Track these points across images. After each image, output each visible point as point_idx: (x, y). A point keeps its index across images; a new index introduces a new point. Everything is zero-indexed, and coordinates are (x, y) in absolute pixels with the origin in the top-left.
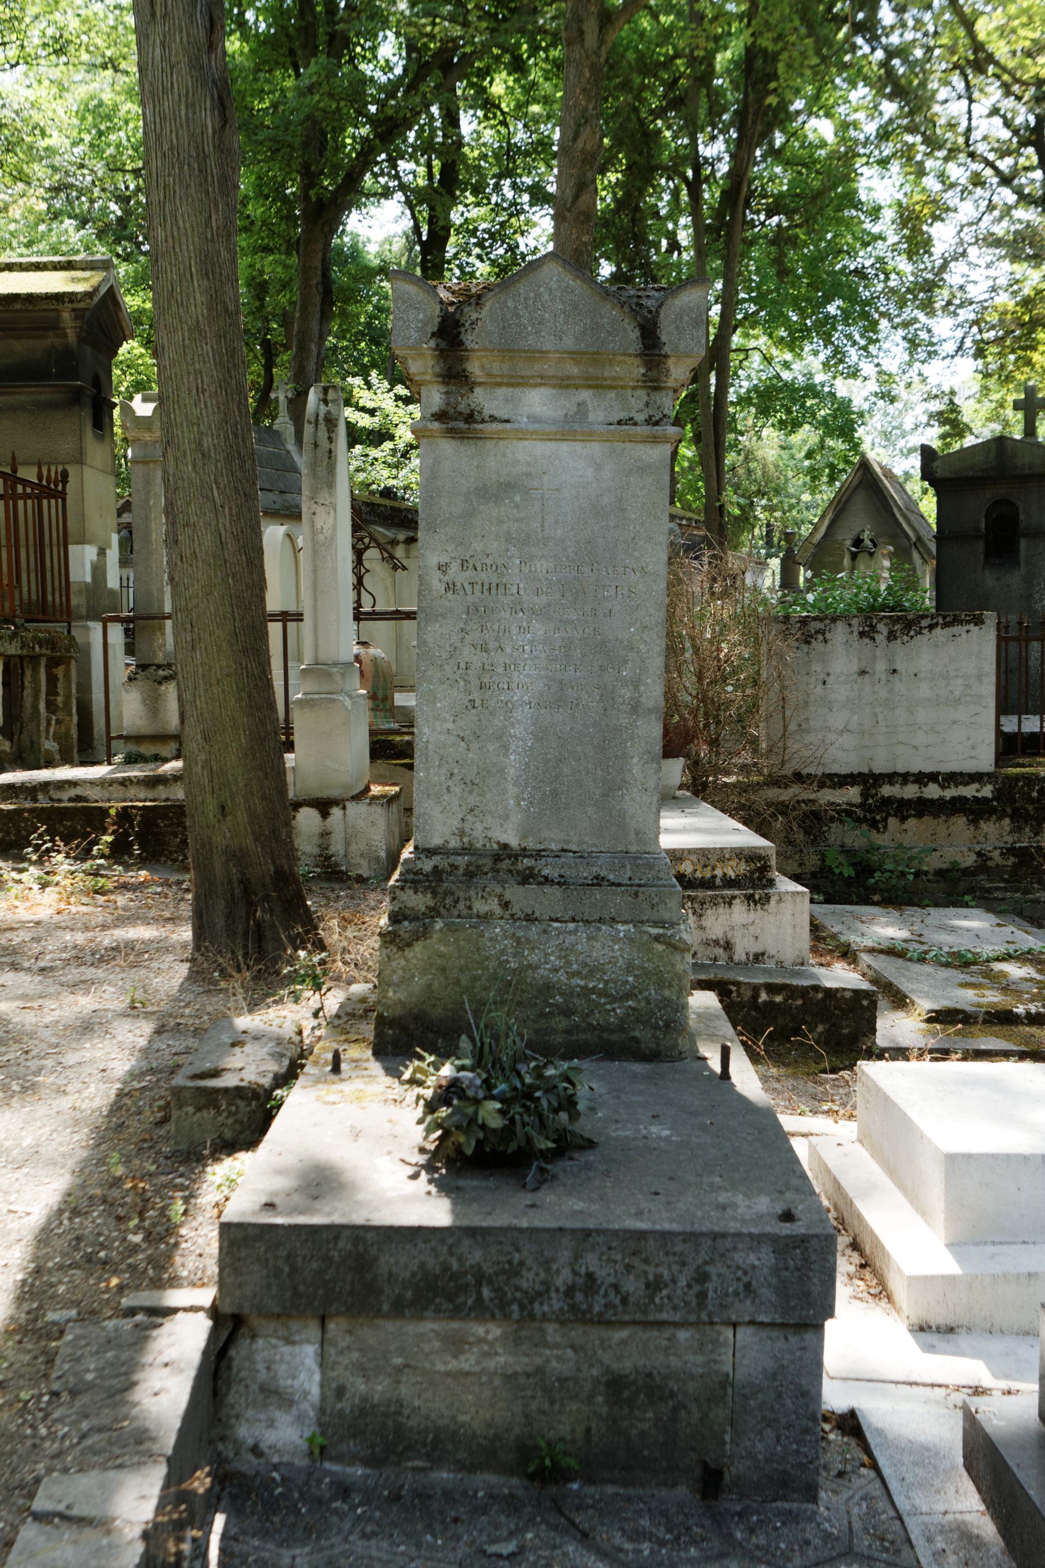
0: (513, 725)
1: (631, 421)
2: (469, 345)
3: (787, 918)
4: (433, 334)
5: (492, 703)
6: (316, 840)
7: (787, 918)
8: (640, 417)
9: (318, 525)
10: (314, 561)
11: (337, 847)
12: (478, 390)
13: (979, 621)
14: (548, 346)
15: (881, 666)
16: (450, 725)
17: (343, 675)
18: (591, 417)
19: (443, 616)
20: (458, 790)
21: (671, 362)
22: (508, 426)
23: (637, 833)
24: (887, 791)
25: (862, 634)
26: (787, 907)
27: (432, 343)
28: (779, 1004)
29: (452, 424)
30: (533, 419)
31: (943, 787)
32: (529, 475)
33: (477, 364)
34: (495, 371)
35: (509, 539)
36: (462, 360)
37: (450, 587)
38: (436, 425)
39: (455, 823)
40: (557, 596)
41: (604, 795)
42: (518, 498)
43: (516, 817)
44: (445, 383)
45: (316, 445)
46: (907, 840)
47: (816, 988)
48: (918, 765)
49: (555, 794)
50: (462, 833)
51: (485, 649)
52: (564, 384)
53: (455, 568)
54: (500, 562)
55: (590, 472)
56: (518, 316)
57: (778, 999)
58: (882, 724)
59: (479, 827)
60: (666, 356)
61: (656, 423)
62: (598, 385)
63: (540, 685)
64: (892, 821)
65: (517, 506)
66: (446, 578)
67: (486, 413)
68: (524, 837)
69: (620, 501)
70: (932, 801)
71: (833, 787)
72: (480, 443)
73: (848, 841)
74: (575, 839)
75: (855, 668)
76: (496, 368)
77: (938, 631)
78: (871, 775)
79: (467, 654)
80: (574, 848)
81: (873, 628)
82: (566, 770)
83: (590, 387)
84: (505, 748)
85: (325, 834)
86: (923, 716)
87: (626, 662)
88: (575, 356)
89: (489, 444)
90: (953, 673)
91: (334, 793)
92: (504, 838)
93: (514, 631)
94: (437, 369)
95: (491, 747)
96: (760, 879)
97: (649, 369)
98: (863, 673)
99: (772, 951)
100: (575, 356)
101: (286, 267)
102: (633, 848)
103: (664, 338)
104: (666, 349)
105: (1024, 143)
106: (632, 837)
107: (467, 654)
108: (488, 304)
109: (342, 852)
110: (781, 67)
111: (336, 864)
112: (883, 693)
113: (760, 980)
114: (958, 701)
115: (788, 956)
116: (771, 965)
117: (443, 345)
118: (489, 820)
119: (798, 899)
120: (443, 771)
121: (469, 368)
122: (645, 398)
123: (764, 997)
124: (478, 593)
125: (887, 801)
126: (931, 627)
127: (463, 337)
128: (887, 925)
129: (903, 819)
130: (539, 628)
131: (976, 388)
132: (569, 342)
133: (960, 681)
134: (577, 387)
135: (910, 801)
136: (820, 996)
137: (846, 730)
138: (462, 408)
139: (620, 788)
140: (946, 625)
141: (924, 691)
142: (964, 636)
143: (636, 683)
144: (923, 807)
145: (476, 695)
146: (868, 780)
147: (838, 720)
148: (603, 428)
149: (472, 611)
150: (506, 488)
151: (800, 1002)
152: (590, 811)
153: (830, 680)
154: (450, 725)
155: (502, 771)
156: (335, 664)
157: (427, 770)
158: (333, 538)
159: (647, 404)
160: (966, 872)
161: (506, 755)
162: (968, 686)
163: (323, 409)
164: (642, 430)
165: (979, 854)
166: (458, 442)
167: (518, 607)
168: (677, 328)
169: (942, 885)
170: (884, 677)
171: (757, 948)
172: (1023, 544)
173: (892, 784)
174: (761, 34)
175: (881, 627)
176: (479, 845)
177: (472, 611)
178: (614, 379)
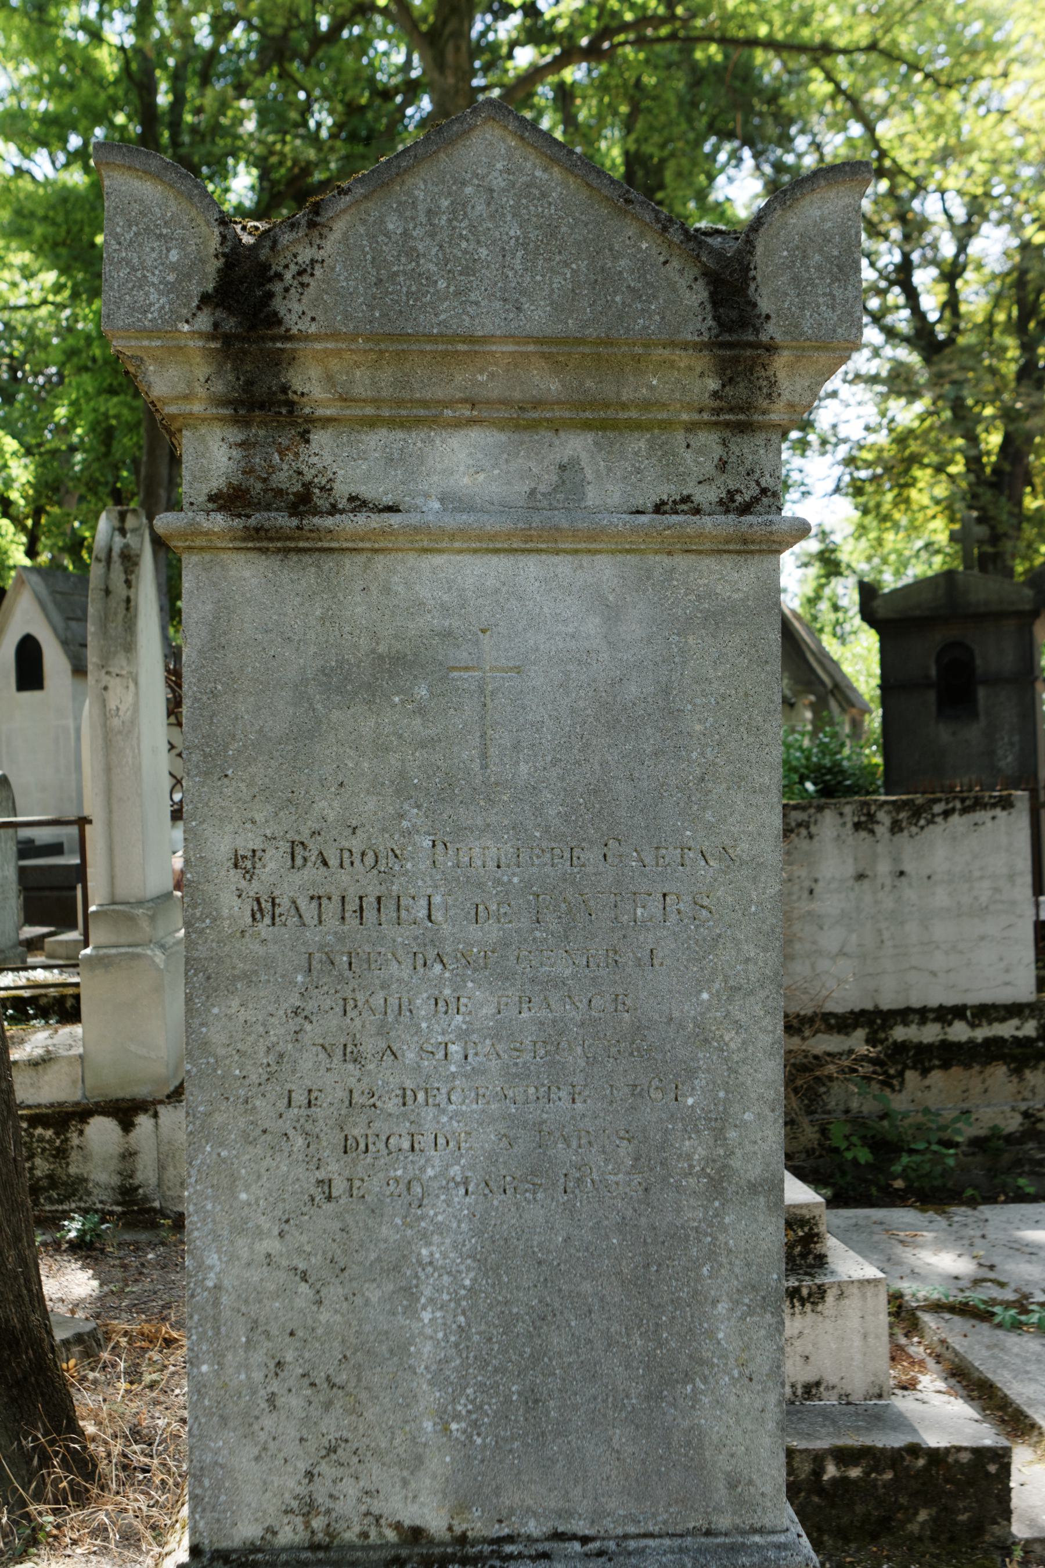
0: (425, 1237)
1: (686, 505)
2: (294, 323)
3: (853, 1322)
4: (205, 299)
5: (375, 1185)
6: (114, 1164)
7: (853, 1322)
8: (707, 495)
9: (112, 704)
10: (107, 755)
11: (146, 1174)
12: (319, 438)
13: (1006, 804)
14: (486, 325)
15: (884, 868)
16: (272, 1245)
17: (152, 918)
18: (592, 496)
19: (249, 978)
20: (295, 1402)
21: (780, 363)
22: (395, 519)
23: (732, 1485)
24: (900, 1033)
25: (857, 826)
26: (853, 1304)
27: (204, 321)
28: (855, 1482)
29: (257, 518)
30: (452, 501)
31: (973, 1026)
32: (447, 634)
33: (315, 372)
34: (359, 390)
35: (402, 788)
36: (278, 361)
37: (264, 909)
38: (219, 521)
39: (291, 1484)
40: (525, 923)
41: (652, 1397)
42: (423, 692)
43: (439, 1462)
44: (240, 422)
45: (107, 592)
46: (932, 1100)
47: (914, 1450)
48: (938, 996)
49: (533, 1400)
50: (309, 1508)
51: (352, 1055)
52: (525, 418)
53: (274, 862)
54: (383, 844)
55: (593, 625)
56: (413, 255)
57: (855, 1473)
58: (889, 943)
59: (350, 1489)
60: (771, 348)
61: (746, 509)
62: (604, 420)
63: (488, 1137)
64: (910, 1075)
65: (421, 711)
66: (254, 888)
67: (342, 490)
68: (461, 1508)
69: (666, 691)
70: (959, 1045)
71: (830, 1029)
72: (329, 563)
73: (854, 1105)
74: (584, 1506)
75: (850, 870)
76: (361, 382)
77: (955, 818)
78: (878, 1012)
79: (309, 1068)
80: (581, 1527)
81: (871, 817)
82: (558, 1342)
83: (587, 426)
84: (410, 1292)
85: (129, 1155)
86: (941, 931)
87: (692, 1073)
88: (554, 349)
89: (351, 565)
90: (977, 874)
91: (141, 1091)
92: (410, 1515)
93: (423, 1006)
94: (219, 387)
95: (374, 1294)
96: (804, 1256)
97: (729, 381)
98: (860, 877)
99: (832, 1379)
100: (554, 349)
101: (132, 409)
102: (724, 1522)
103: (765, 305)
104: (772, 330)
105: (892, 283)
106: (721, 1493)
107: (309, 1068)
108: (340, 226)
109: (153, 1181)
110: (668, 176)
111: (146, 1199)
112: (889, 904)
113: (822, 1444)
114: (984, 911)
115: (858, 1385)
116: (830, 1400)
117: (230, 324)
118: (375, 1473)
119: (870, 1291)
120: (258, 1357)
121: (297, 383)
122: (718, 451)
123: (831, 1471)
124: (331, 921)
125: (901, 1048)
126: (947, 814)
127: (279, 305)
128: (940, 1245)
129: (925, 1072)
130: (481, 1001)
131: (850, 529)
132: (537, 316)
133: (986, 884)
134: (556, 427)
135: (930, 1046)
136: (921, 1462)
137: (842, 953)
138: (282, 478)
139: (688, 1378)
140: (965, 811)
141: (941, 898)
142: (989, 824)
143: (718, 1124)
144: (949, 1055)
145: (334, 1168)
146: (874, 1020)
147: (831, 939)
148: (621, 521)
149: (318, 965)
150: (388, 671)
151: (889, 1476)
152: (619, 1435)
153: (818, 888)
154: (272, 1245)
155: (401, 1349)
156: (140, 903)
158: (134, 721)
159: (722, 466)
160: (1009, 1139)
161: (411, 1312)
162: (997, 890)
163: (118, 541)
164: (717, 525)
165: (1026, 1115)
166: (273, 562)
167: (428, 953)
168: (796, 280)
169: (979, 1158)
170: (888, 882)
171: (807, 1375)
172: (981, 693)
173: (906, 1024)
174: (646, 140)
175: (882, 816)
176: (350, 1536)
177: (318, 965)
178: (646, 405)
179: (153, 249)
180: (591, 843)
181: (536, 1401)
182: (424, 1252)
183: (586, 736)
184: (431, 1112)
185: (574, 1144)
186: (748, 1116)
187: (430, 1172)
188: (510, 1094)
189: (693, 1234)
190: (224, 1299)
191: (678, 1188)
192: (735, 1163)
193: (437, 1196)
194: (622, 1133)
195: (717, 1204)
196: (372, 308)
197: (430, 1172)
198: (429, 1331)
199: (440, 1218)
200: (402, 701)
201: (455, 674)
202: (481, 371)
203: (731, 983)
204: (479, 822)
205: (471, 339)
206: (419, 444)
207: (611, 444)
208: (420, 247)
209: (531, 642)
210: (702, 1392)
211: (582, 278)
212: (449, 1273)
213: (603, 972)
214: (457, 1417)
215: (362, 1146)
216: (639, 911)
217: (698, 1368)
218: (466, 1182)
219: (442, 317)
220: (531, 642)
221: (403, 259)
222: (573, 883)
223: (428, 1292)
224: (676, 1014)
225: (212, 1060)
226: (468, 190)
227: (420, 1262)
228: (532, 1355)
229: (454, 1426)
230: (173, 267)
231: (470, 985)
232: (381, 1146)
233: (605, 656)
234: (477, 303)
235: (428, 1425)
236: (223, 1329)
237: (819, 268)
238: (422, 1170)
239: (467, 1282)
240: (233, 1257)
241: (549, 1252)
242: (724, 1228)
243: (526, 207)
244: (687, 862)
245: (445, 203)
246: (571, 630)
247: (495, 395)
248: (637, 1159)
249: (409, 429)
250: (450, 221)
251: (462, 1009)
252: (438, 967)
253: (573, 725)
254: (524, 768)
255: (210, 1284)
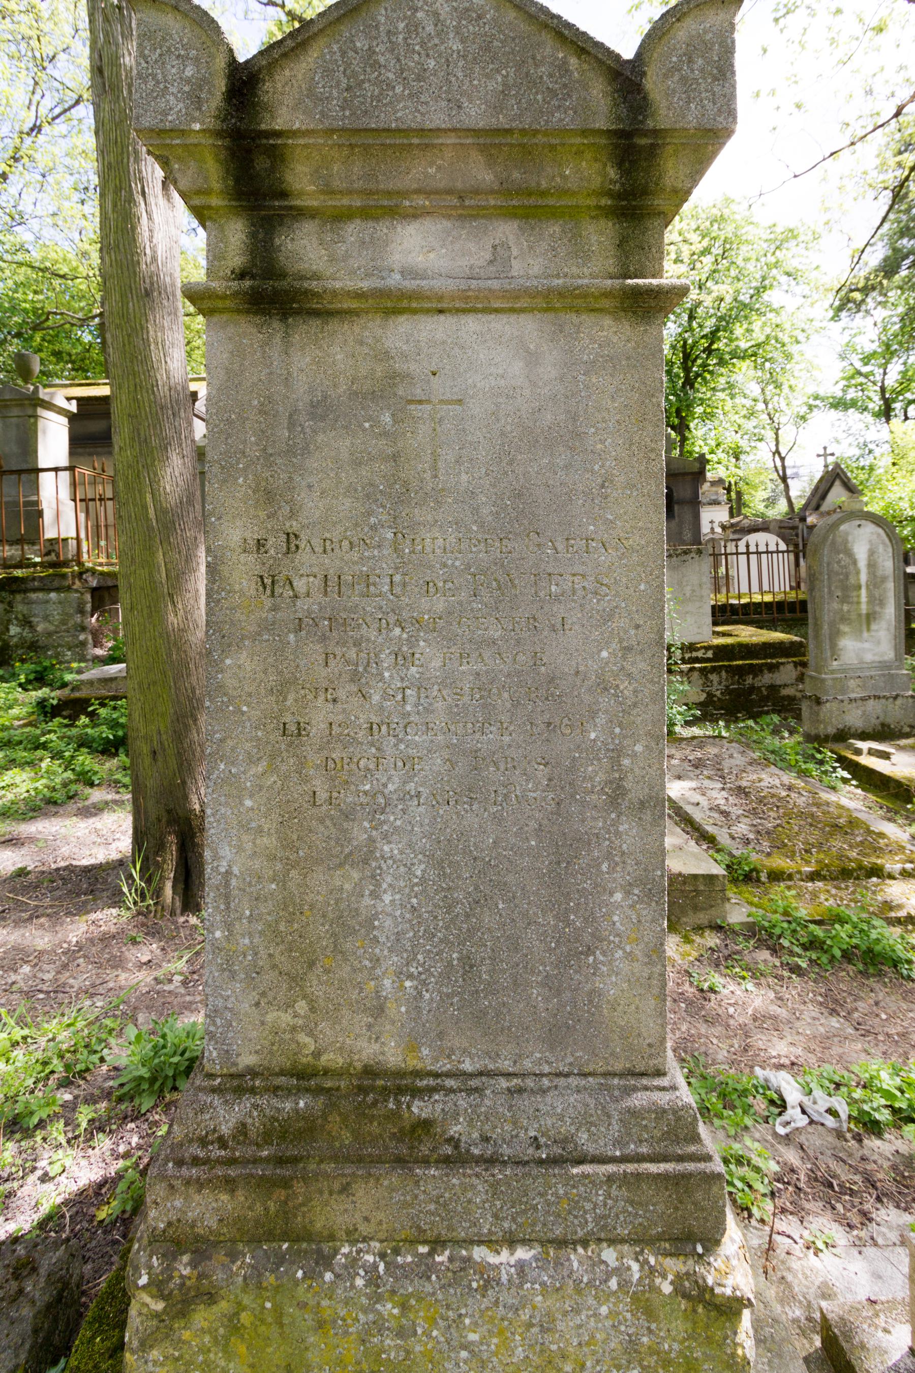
40: (463, 595)
42: (387, 418)
49: (469, 964)
55: (517, 368)
56: (376, 66)
68: (413, 1047)
87: (593, 714)
88: (490, 140)
93: (387, 660)
132: (475, 114)
139: (589, 951)
157: (229, 926)
162: (694, 591)
168: (684, 80)
179: (173, 67)
180: (516, 534)
181: (471, 967)
182: (386, 848)
183: (512, 453)
184: (393, 740)
185: (502, 768)
186: (639, 748)
187: (391, 787)
188: (453, 728)
189: (595, 840)
190: (234, 882)
191: (583, 803)
192: (627, 784)
193: (396, 806)
194: (539, 760)
195: (613, 816)
196: (343, 109)
197: (391, 787)
198: (389, 909)
199: (398, 823)
200: (371, 426)
201: (412, 407)
202: (431, 165)
203: (625, 644)
204: (429, 518)
205: (422, 132)
206: (385, 230)
207: (533, 229)
208: (382, 60)
209: (470, 381)
210: (602, 962)
211: (511, 82)
212: (405, 865)
213: (524, 635)
214: (410, 977)
215: (339, 766)
216: (553, 588)
217: (597, 944)
218: (418, 795)
219: (399, 114)
220: (470, 381)
221: (368, 69)
222: (502, 565)
223: (389, 879)
224: (582, 668)
225: (225, 699)
226: (420, 15)
227: (383, 857)
228: (468, 930)
229: (408, 984)
230: (188, 81)
231: (422, 643)
232: (354, 766)
233: (527, 392)
234: (426, 103)
235: (387, 983)
236: (232, 905)
237: (702, 70)
238: (385, 785)
239: (419, 873)
240: (240, 849)
241: (482, 850)
242: (618, 834)
243: (466, 27)
244: (591, 550)
245: (401, 26)
246: (500, 371)
247: (441, 185)
248: (550, 780)
249: (376, 219)
250: (405, 39)
251: (417, 662)
252: (397, 631)
253: (503, 444)
254: (464, 477)
255: (223, 870)
